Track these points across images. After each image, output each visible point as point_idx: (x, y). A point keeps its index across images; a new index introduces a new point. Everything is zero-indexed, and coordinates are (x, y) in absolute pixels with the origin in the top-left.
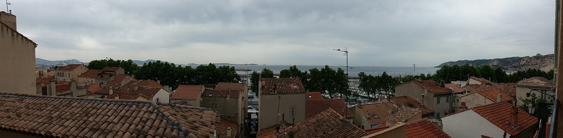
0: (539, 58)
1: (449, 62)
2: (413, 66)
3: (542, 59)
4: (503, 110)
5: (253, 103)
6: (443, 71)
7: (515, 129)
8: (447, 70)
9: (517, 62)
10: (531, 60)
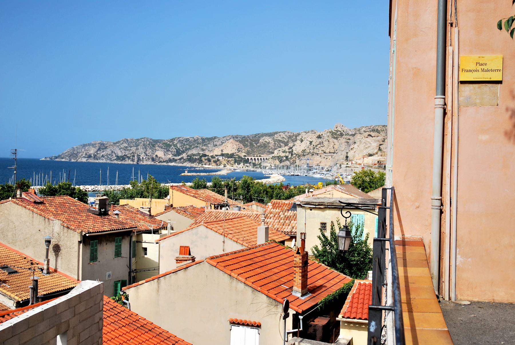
0: (342, 135)
3: (348, 137)
4: (273, 260)
7: (303, 298)
9: (286, 144)
10: (320, 140)
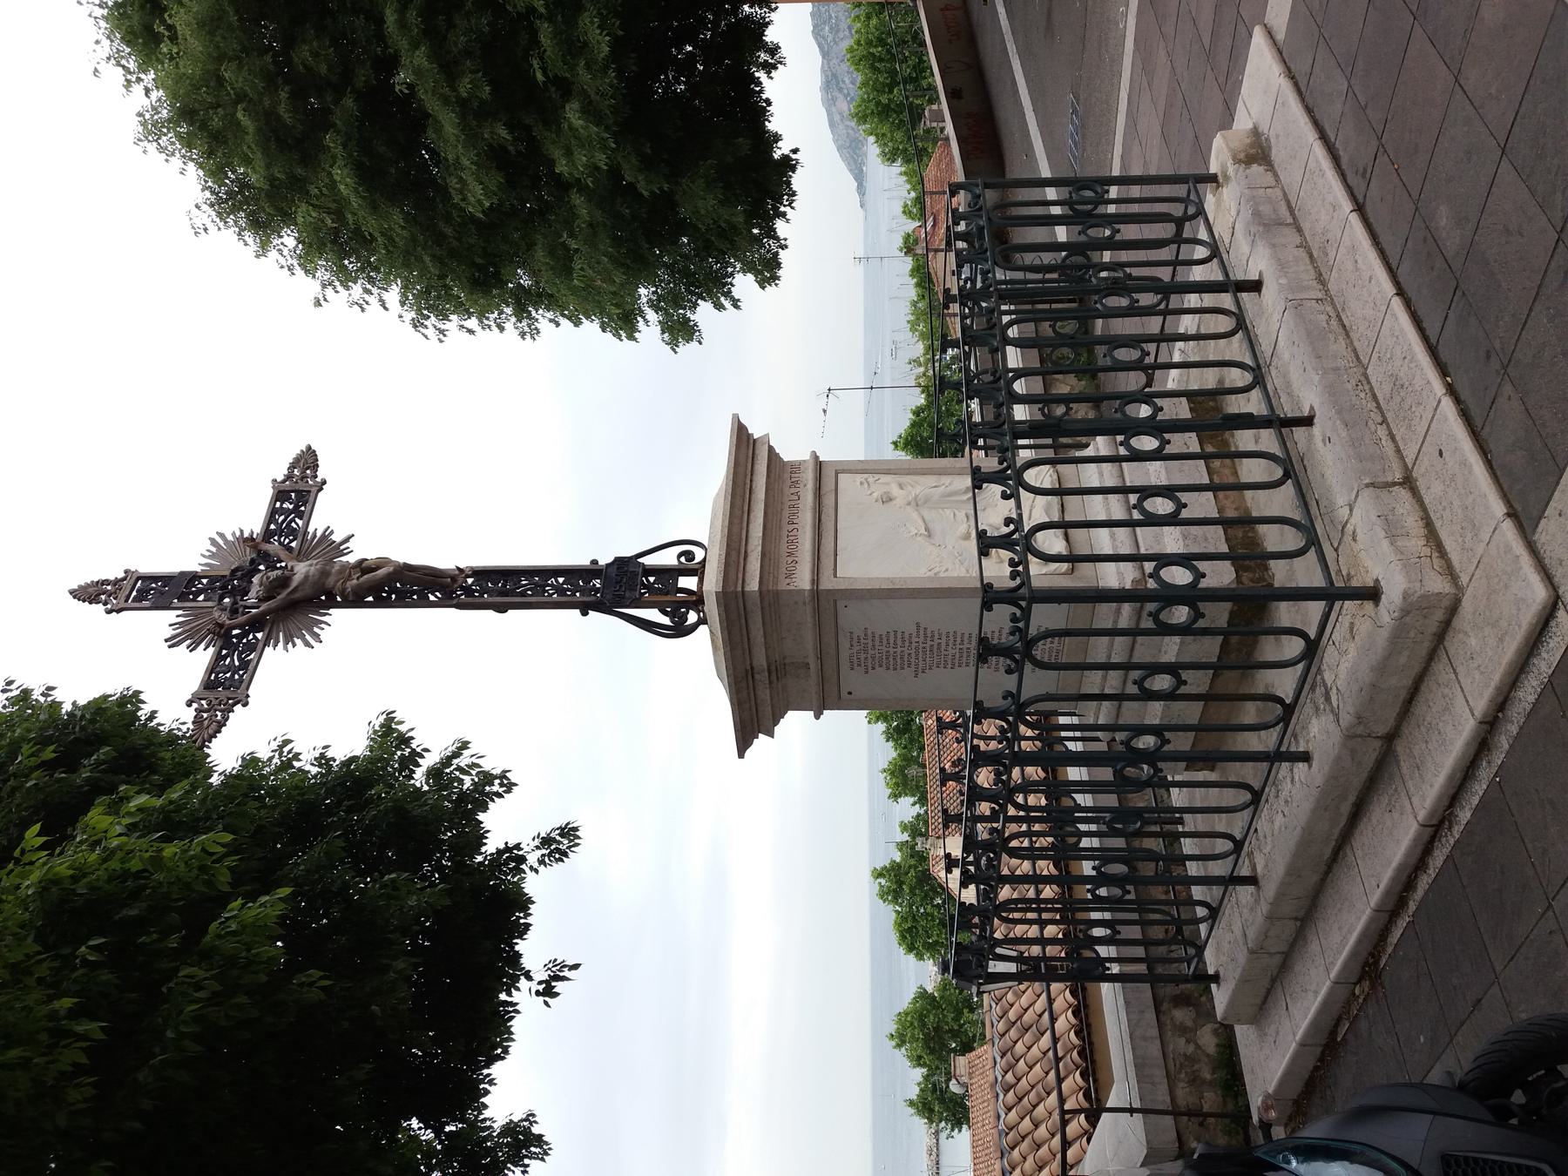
1: (829, 103)
2: (860, 268)
5: (1078, 734)
6: (885, 129)
8: (878, 103)
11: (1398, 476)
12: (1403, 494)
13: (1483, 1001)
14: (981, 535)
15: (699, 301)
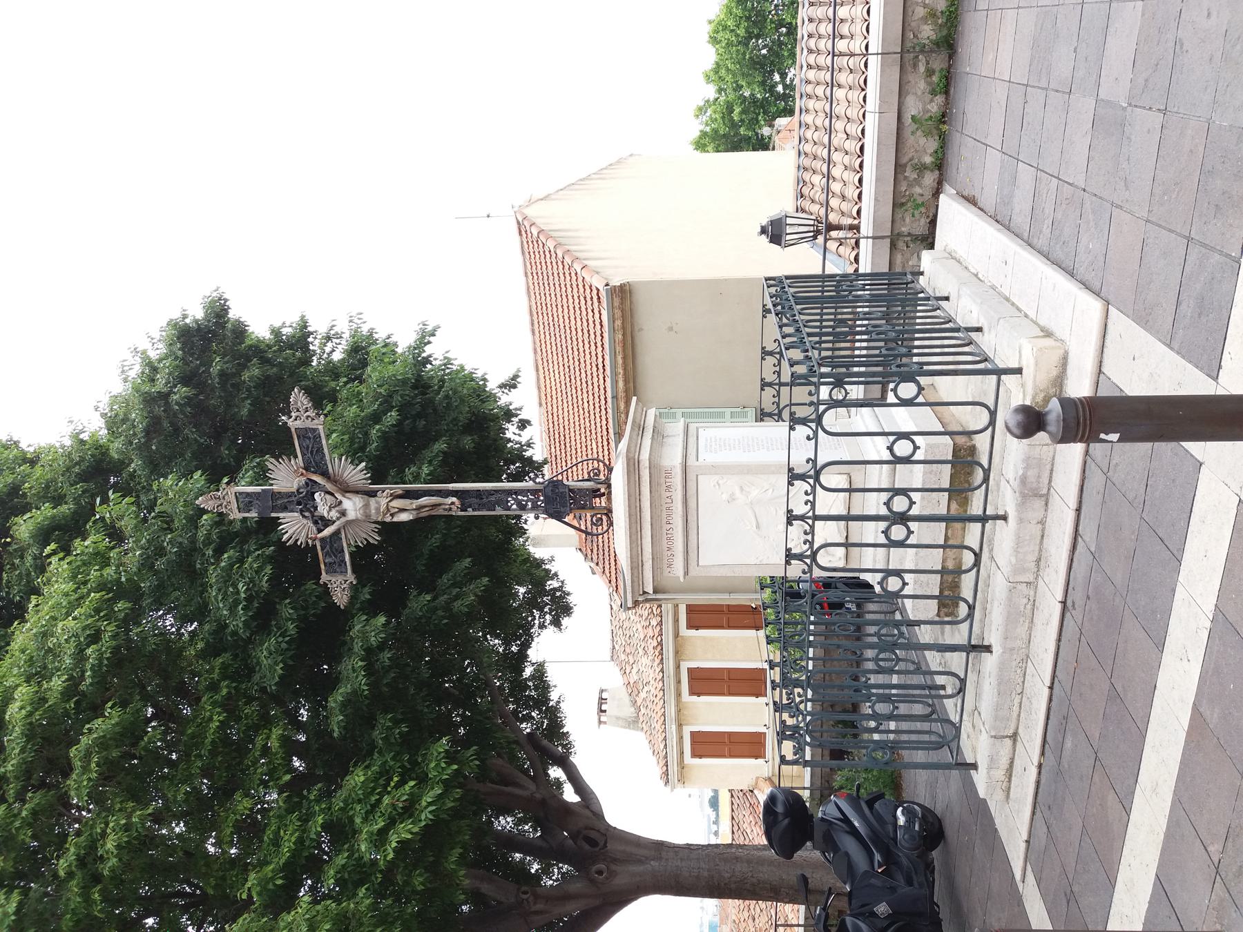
11: (1010, 732)
12: (1008, 742)
13: (1020, 731)
14: (788, 550)
15: (613, 867)
